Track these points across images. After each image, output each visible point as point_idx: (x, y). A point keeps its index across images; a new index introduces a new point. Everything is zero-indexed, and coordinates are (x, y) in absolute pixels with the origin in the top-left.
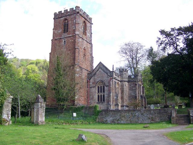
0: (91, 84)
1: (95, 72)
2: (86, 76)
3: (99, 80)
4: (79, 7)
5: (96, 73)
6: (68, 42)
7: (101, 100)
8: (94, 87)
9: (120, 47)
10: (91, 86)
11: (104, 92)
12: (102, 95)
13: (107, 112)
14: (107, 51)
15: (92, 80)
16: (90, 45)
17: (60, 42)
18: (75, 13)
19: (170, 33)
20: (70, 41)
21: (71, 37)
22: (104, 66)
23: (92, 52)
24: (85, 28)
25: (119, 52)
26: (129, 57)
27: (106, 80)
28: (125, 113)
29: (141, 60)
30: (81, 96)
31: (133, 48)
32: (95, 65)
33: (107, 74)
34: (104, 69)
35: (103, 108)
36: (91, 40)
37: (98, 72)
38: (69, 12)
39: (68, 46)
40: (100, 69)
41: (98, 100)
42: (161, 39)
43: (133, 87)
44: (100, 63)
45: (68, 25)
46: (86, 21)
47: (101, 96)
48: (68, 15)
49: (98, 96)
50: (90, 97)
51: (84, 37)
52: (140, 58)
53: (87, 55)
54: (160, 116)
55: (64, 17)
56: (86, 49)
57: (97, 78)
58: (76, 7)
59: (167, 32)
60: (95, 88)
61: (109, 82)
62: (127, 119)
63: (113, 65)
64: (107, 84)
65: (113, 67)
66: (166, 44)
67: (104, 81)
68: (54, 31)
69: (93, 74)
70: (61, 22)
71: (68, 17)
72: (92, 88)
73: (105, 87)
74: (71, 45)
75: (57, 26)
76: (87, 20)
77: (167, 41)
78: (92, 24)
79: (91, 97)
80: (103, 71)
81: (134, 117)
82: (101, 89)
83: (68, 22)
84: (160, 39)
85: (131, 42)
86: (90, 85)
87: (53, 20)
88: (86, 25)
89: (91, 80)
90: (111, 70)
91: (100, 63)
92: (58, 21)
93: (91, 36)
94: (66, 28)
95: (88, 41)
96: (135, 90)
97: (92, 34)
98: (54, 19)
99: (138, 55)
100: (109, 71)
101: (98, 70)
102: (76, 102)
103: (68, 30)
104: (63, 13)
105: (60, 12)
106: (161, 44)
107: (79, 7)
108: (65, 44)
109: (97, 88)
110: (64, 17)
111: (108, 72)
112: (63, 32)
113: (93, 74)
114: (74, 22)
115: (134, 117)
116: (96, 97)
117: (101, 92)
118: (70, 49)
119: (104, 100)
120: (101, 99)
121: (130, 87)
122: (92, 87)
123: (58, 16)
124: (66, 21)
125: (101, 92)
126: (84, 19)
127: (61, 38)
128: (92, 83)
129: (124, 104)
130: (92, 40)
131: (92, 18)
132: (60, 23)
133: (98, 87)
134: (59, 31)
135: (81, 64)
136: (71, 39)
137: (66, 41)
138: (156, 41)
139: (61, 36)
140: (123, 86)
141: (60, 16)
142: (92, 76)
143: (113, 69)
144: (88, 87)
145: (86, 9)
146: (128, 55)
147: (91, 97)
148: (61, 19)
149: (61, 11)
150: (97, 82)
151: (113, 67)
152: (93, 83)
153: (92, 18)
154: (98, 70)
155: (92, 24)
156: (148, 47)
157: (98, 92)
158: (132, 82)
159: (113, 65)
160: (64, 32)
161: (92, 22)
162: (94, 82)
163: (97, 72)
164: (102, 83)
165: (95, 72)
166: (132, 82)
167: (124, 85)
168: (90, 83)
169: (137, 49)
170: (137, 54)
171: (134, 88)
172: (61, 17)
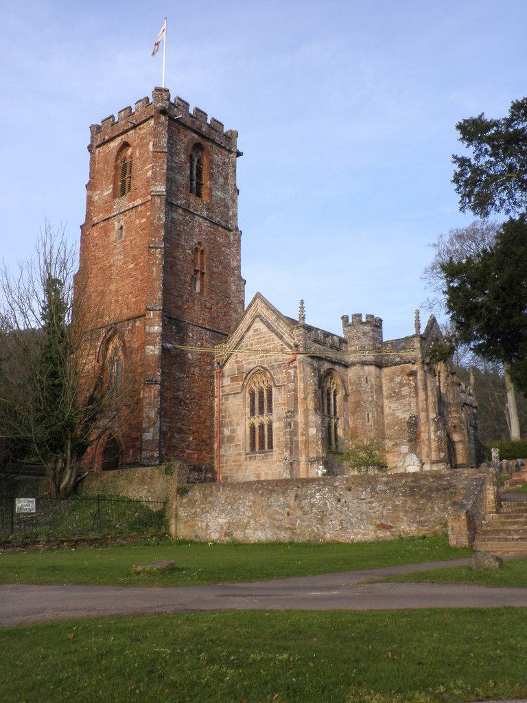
6: (129, 230)
7: (262, 447)
21: (140, 209)
33: (281, 338)
37: (251, 332)
39: (131, 241)
53: (212, 273)
55: (120, 138)
56: (207, 249)
63: (302, 302)
65: (302, 308)
68: (90, 193)
70: (113, 157)
73: (274, 390)
74: (139, 240)
76: (213, 141)
78: (239, 154)
81: (305, 513)
92: (102, 154)
98: (90, 148)
109: (248, 395)
110: (119, 135)
112: (119, 193)
115: (305, 513)
117: (261, 412)
119: (271, 446)
126: (196, 136)
133: (252, 394)
134: (105, 194)
136: (140, 216)
139: (110, 209)
141: (107, 138)
149: (112, 117)
151: (302, 308)
155: (239, 154)
159: (302, 302)
161: (240, 147)
166: (396, 364)
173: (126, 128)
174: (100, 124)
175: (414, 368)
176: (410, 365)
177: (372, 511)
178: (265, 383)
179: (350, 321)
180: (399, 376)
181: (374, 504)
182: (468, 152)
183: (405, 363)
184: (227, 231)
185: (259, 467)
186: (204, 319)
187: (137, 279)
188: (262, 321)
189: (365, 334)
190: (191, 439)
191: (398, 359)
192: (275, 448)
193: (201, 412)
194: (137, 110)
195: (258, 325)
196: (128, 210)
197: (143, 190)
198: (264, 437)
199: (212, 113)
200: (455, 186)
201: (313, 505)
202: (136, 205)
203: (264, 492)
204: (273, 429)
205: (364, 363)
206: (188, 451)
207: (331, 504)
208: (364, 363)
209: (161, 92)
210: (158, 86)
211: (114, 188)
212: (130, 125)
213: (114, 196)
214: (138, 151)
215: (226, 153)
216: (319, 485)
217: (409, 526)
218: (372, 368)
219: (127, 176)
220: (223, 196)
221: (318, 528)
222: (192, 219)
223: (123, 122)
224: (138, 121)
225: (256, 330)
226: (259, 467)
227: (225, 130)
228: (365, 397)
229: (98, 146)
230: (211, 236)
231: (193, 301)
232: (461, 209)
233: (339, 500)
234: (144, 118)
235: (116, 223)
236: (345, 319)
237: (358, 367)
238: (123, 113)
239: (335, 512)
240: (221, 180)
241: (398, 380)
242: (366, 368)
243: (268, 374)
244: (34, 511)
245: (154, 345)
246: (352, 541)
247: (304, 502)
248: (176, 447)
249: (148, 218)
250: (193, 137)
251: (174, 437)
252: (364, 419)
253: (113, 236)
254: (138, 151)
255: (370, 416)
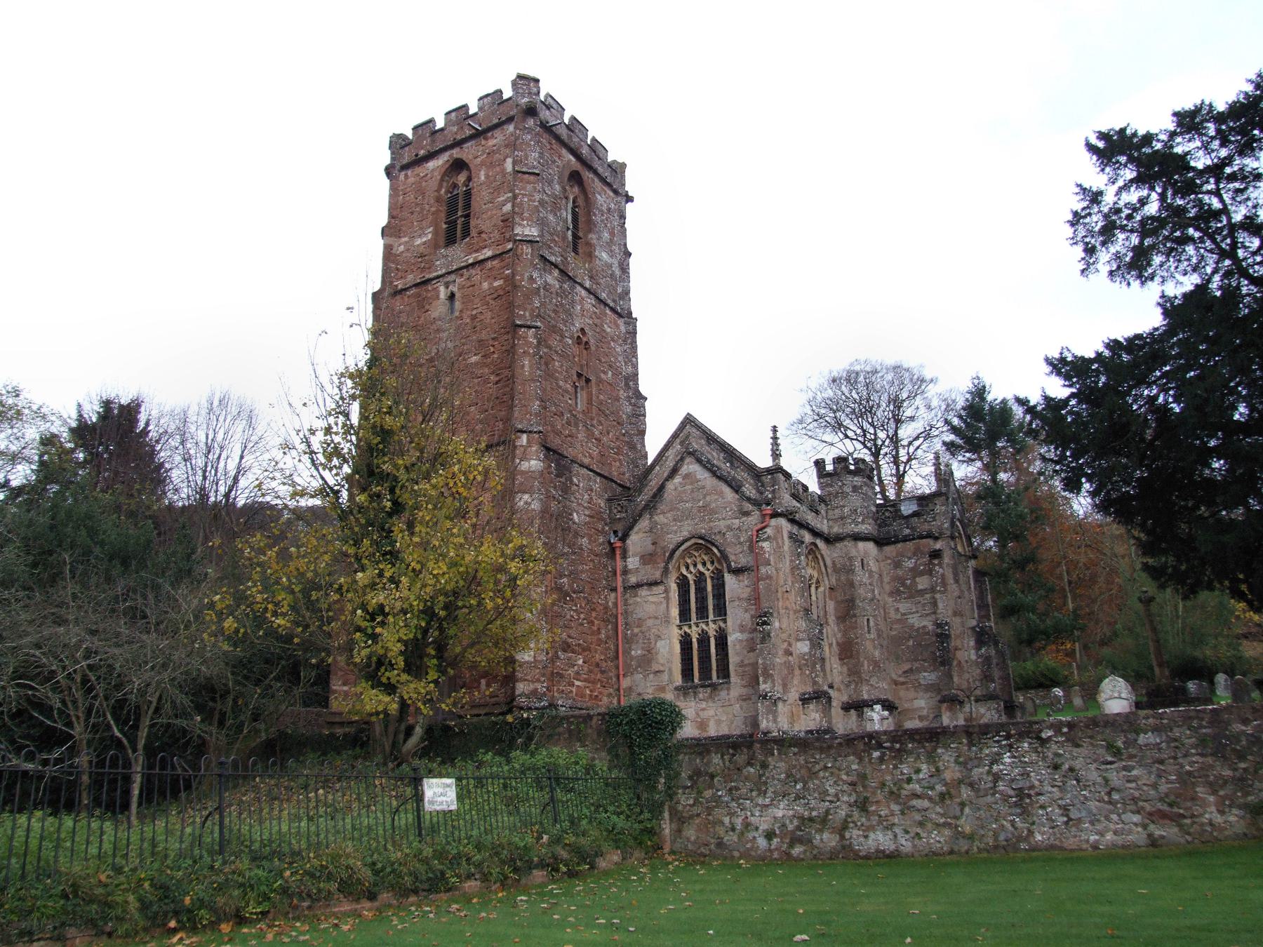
0: (630, 567)
1: (654, 483)
2: (596, 516)
3: (686, 534)
4: (537, 81)
5: (661, 488)
6: (467, 300)
8: (656, 583)
9: (804, 398)
10: (633, 580)
11: (721, 610)
12: (712, 633)
13: (741, 759)
14: (730, 345)
15: (637, 541)
16: (621, 322)
17: (423, 304)
18: (510, 120)
19: (1168, 145)
20: (485, 285)
21: (489, 264)
22: (711, 438)
23: (635, 366)
24: (582, 219)
25: (801, 422)
26: (859, 446)
27: (730, 528)
28: (899, 755)
29: (919, 452)
30: (566, 647)
31: (875, 397)
32: (654, 443)
33: (737, 489)
34: (717, 458)
35: (719, 722)
36: (627, 293)
37: (677, 479)
38: (476, 114)
39: (474, 318)
40: (688, 460)
41: (687, 672)
42: (1109, 199)
43: (915, 572)
44: (689, 421)
45: (468, 194)
46: (587, 175)
47: (704, 639)
48: (472, 137)
49: (686, 643)
50: (627, 652)
51: (578, 268)
52: (916, 443)
53: (600, 381)
54: (1227, 773)
56: (592, 341)
57: (673, 525)
58: (514, 83)
59: (1148, 139)
60: (661, 588)
61: (753, 546)
62: (918, 817)
63: (775, 429)
64: (739, 558)
65: (775, 438)
66: (1148, 228)
67: (718, 539)
68: (391, 240)
69: (642, 499)
70: (433, 184)
71: (468, 152)
72: (643, 592)
73: (729, 579)
75: (405, 214)
76: (595, 172)
77: (1152, 208)
78: (629, 199)
79: (637, 652)
80: (707, 475)
82: (701, 599)
83: (469, 179)
84: (1095, 197)
85: (857, 368)
86: (625, 572)
87: (386, 183)
88: (587, 199)
89: (628, 542)
90: (763, 460)
91: (689, 421)
92: (411, 180)
93: (625, 269)
94: (456, 221)
95: (604, 296)
96: (933, 590)
97: (631, 260)
98: (389, 171)
99: (901, 433)
100: (750, 467)
101: (674, 471)
102: (521, 687)
103: (473, 223)
104: (442, 130)
105: (425, 127)
106: (1108, 231)
107: (537, 81)
108: (452, 309)
109: (674, 587)
111: (741, 475)
112: (442, 241)
113: (642, 499)
114: (503, 172)
116: (668, 649)
117: (702, 612)
118: (484, 335)
119: (724, 672)
120: (704, 664)
121: (896, 579)
122: (639, 585)
123: (407, 155)
124: (462, 178)
125: (702, 612)
127: (426, 282)
128: (642, 557)
129: (865, 688)
130: (632, 295)
131: (623, 166)
132: (421, 192)
133: (683, 584)
134: (418, 242)
135: (558, 433)
137: (457, 295)
138: (1070, 217)
140: (851, 571)
141: (422, 152)
142: (640, 516)
143: (776, 455)
144: (614, 590)
145: (578, 97)
146: (850, 434)
147: (637, 652)
148: (431, 165)
149: (431, 121)
150: (671, 547)
151: (775, 438)
152: (647, 559)
153: (623, 166)
154: (674, 471)
155: (629, 199)
156: (952, 386)
157: (684, 615)
158: (910, 545)
159: (775, 429)
160: (450, 240)
161: (630, 187)
162: (651, 548)
163: (670, 486)
164: (709, 551)
165: (654, 483)
166: (906, 539)
167: (857, 564)
168: (624, 557)
169: (897, 403)
170: (897, 428)
171: (923, 583)
172: (431, 156)
173: (459, 137)
174: (410, 135)
175: (938, 546)
176: (931, 541)
177: (1133, 785)
178: (692, 568)
179: (829, 468)
180: (910, 558)
181: (1135, 772)
182: (1095, 178)
183: (921, 537)
184: (615, 316)
185: (703, 710)
186: (591, 456)
187: (487, 381)
188: (699, 461)
189: (855, 489)
190: (580, 662)
191: (907, 531)
192: (733, 678)
193: (594, 614)
194: (481, 109)
195: (691, 467)
196: (467, 267)
197: (496, 235)
198: (709, 657)
199: (596, 130)
200: (1069, 231)
201: (997, 777)
202: (482, 257)
203: (883, 754)
204: (729, 643)
205: (857, 537)
206: (577, 683)
207: (1039, 775)
208: (857, 537)
209: (525, 82)
210: (523, 72)
211: (435, 233)
212: (468, 132)
213: (434, 245)
214: (482, 173)
215: (611, 194)
216: (1008, 737)
217: (1222, 812)
218: (870, 546)
219: (460, 213)
220: (610, 261)
221: (1013, 823)
222: (573, 288)
223: (455, 129)
224: (485, 126)
225: (687, 476)
226: (703, 710)
227: (611, 158)
228: (861, 591)
229: (405, 167)
230: (596, 321)
231: (576, 425)
232: (1083, 271)
233: (1056, 767)
234: (495, 121)
235: (442, 289)
236: (819, 464)
237: (848, 544)
238: (453, 114)
239: (1050, 789)
240: (606, 235)
241: (910, 564)
242: (861, 544)
243: (715, 550)
244: (454, 807)
245: (531, 493)
246: (1095, 847)
247: (976, 772)
248: (561, 676)
249: (506, 279)
250: (569, 161)
251: (558, 658)
252: (862, 628)
253: (439, 308)
254: (482, 173)
255: (872, 624)
